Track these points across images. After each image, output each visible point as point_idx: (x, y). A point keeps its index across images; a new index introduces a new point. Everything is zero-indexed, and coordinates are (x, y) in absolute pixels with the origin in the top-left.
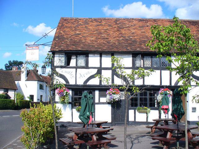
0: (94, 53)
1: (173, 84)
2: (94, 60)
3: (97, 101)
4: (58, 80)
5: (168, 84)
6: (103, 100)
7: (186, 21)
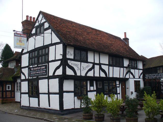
3: (89, 90)
4: (69, 72)
6: (92, 88)
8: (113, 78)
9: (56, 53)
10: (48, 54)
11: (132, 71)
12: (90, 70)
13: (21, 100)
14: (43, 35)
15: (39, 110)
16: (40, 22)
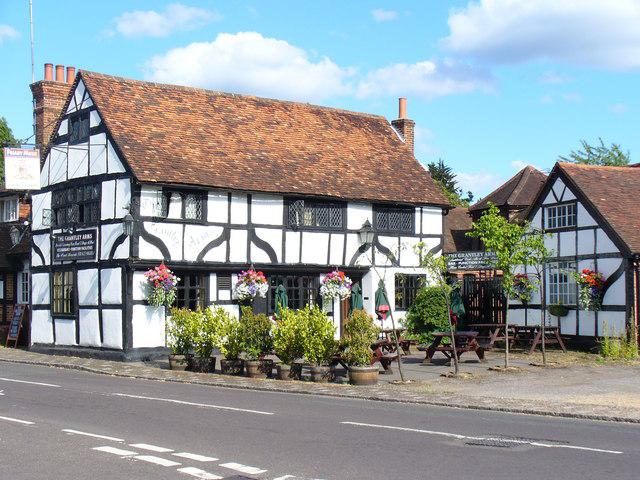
0: (216, 190)
1: (347, 264)
2: (217, 207)
3: (213, 298)
4: (148, 252)
5: (340, 263)
6: (225, 295)
7: (340, 115)
8: (300, 266)
9: (114, 199)
10: (97, 202)
11: (384, 241)
12: (215, 243)
13: (54, 323)
14: (84, 146)
15: (81, 351)
16: (79, 107)
